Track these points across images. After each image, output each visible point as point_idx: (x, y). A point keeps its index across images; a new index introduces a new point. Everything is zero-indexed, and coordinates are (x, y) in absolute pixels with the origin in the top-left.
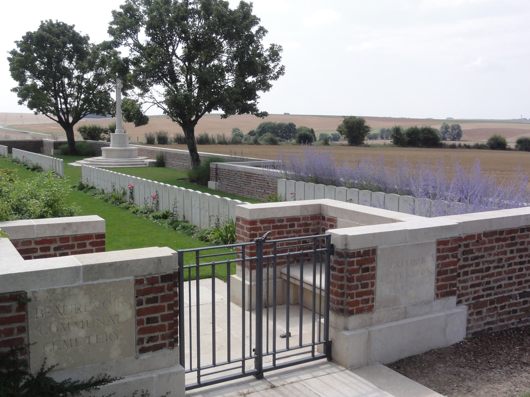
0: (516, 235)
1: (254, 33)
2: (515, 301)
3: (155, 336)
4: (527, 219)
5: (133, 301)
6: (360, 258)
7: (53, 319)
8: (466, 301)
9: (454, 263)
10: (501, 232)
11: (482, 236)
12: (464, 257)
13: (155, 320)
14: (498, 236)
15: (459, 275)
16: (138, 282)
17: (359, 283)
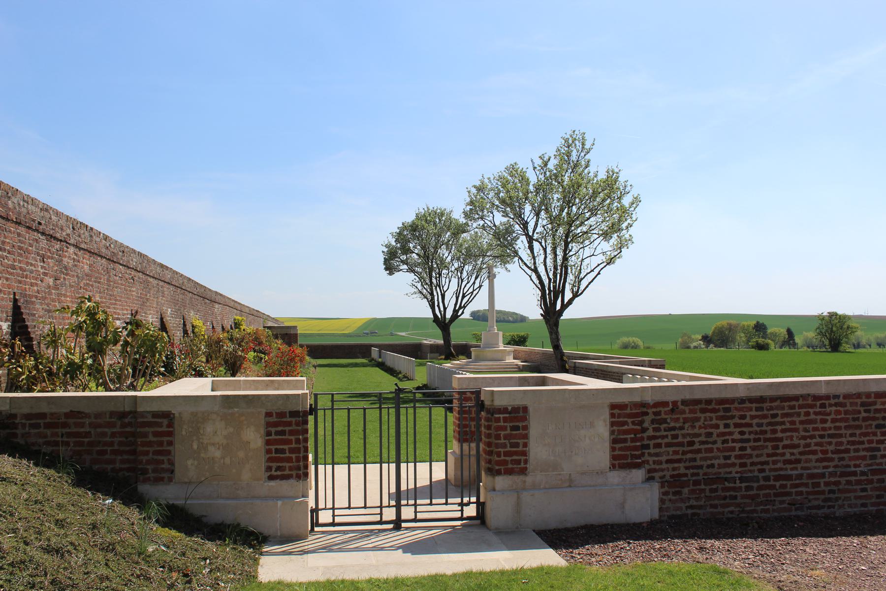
0: (732, 406)
1: (627, 206)
2: (732, 485)
4: (748, 389)
5: (262, 431)
7: (195, 438)
8: (661, 478)
9: (635, 432)
10: (709, 402)
11: (679, 403)
13: (283, 451)
14: (703, 406)
15: (647, 447)
16: (269, 414)
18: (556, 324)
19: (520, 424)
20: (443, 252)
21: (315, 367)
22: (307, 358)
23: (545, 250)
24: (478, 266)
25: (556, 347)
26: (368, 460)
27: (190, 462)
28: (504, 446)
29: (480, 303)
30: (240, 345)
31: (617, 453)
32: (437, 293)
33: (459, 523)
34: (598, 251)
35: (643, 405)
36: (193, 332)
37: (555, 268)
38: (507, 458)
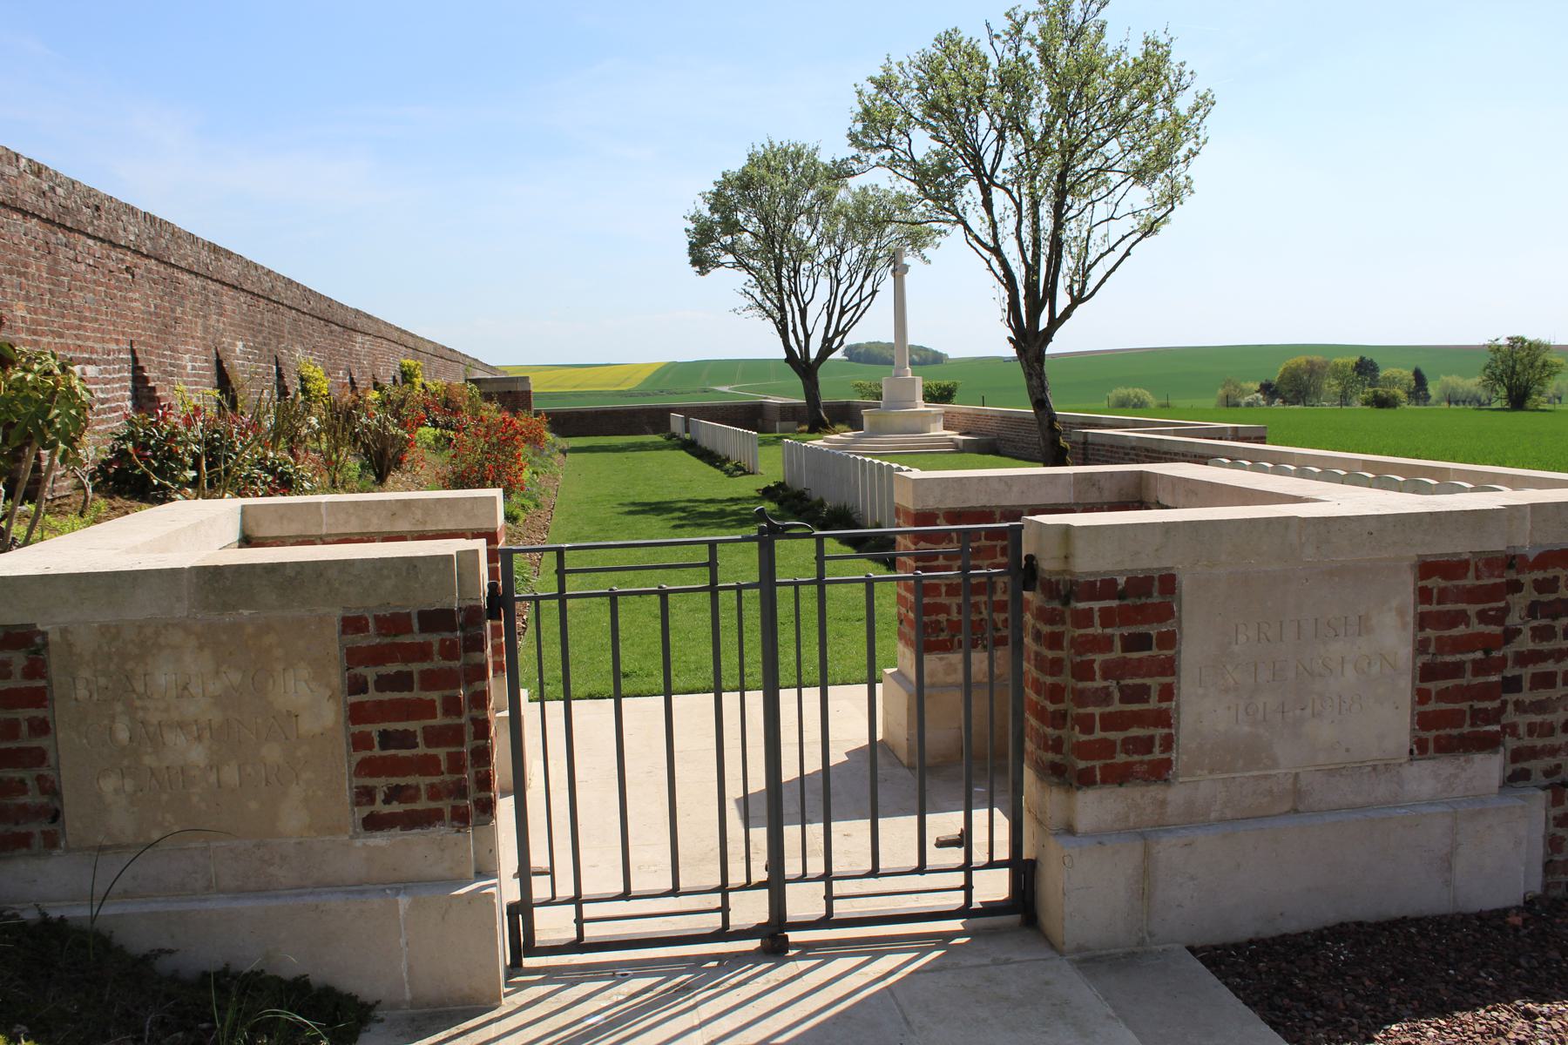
3: (407, 787)
5: (336, 678)
6: (1114, 603)
7: (119, 707)
8: (1548, 773)
9: (1487, 644)
12: (1535, 623)
13: (406, 740)
15: (1513, 684)
16: (352, 624)
17: (1112, 684)
18: (1040, 357)
19: (1153, 630)
20: (802, 228)
21: (564, 452)
22: (549, 436)
23: (1019, 206)
24: (869, 254)
25: (1041, 403)
26: (677, 683)
27: (108, 785)
28: (1104, 697)
29: (873, 328)
30: (396, 414)
31: (1432, 706)
32: (792, 307)
33: (956, 925)
34: (1124, 208)
35: (1511, 561)
36: (305, 391)
37: (1036, 243)
38: (1112, 735)
